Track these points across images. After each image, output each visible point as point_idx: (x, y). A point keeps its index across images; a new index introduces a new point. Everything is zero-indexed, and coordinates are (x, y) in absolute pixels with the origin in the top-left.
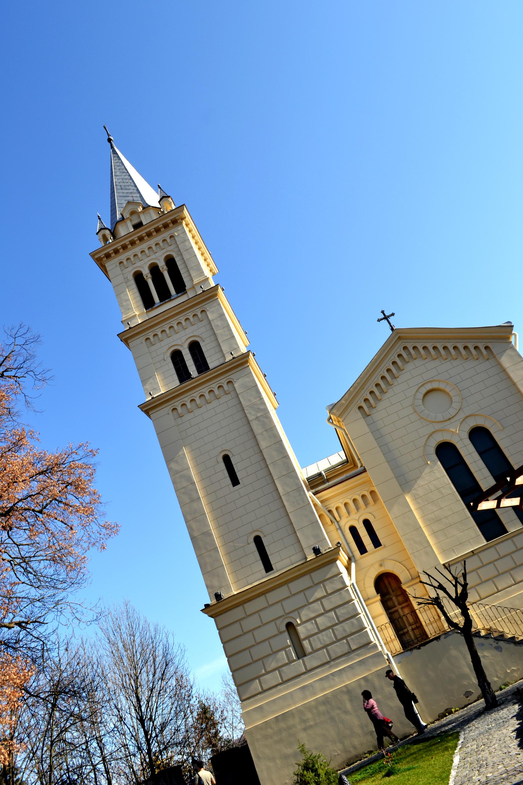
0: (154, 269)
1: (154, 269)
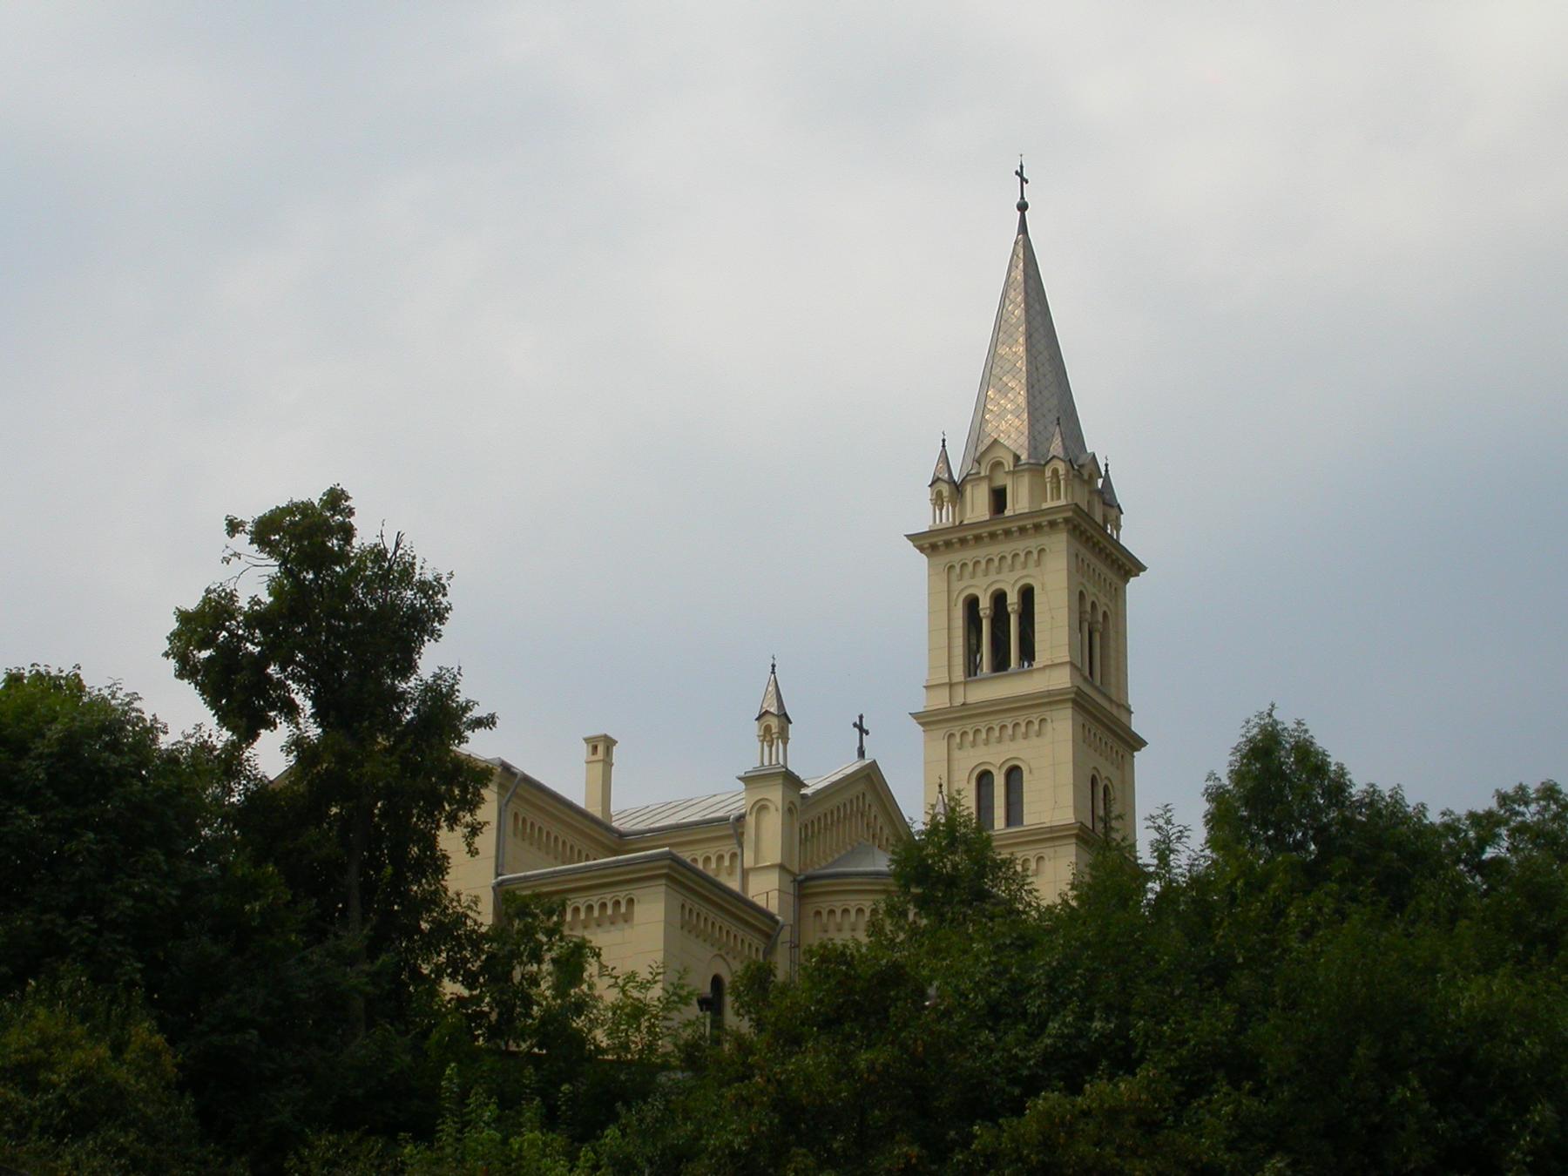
0: (999, 598)
1: (999, 598)
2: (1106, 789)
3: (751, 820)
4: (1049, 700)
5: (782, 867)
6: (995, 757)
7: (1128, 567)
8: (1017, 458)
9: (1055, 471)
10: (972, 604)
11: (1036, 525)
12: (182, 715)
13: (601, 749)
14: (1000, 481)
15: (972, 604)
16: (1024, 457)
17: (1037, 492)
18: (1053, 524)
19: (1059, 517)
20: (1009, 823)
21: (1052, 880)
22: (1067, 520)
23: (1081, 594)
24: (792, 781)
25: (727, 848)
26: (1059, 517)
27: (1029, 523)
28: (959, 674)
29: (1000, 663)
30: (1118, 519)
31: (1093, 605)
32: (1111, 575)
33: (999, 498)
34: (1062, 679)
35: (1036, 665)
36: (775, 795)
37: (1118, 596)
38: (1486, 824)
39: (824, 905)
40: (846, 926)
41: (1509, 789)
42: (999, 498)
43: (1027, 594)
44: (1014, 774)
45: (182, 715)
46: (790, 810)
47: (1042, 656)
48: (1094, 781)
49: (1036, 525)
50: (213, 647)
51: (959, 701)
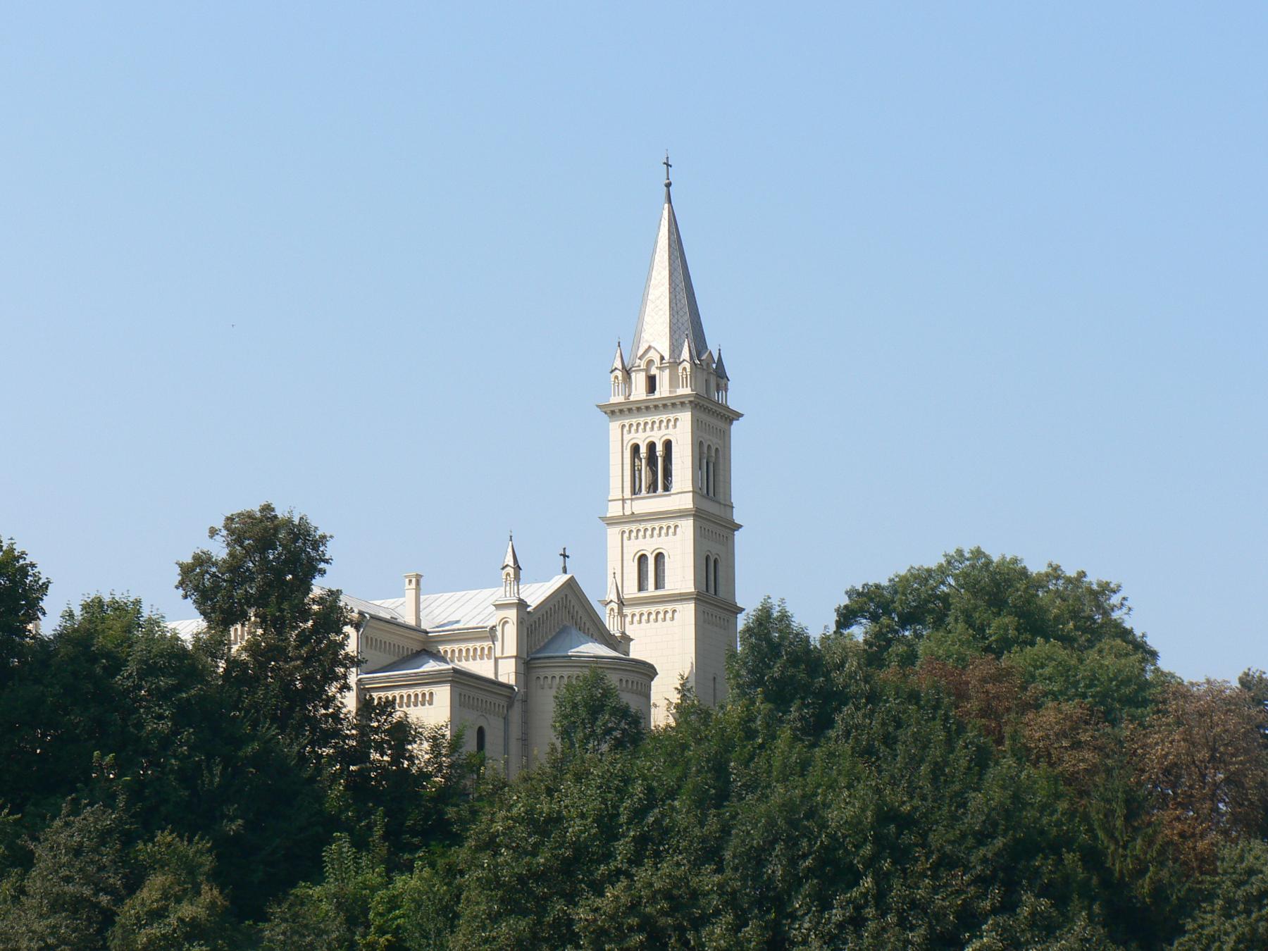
0: (652, 446)
1: (652, 446)
2: (716, 561)
3: (499, 629)
4: (681, 514)
5: (516, 657)
6: (649, 546)
7: (731, 416)
8: (662, 358)
9: (684, 369)
10: (636, 449)
11: (673, 404)
12: (187, 625)
13: (414, 580)
14: (654, 371)
15: (636, 449)
16: (667, 357)
17: (673, 383)
18: (682, 403)
19: (686, 400)
20: (657, 588)
21: (667, 647)
22: (691, 402)
23: (701, 443)
24: (522, 605)
25: (486, 644)
26: (686, 400)
27: (669, 403)
28: (628, 494)
29: (653, 487)
30: (726, 385)
31: (709, 446)
32: (721, 424)
33: (651, 383)
34: (687, 502)
35: (673, 491)
36: (512, 614)
37: (725, 436)
38: (942, 570)
39: (542, 673)
40: (555, 686)
41: (952, 552)
42: (651, 383)
43: (668, 445)
44: (659, 557)
45: (187, 625)
46: (520, 622)
47: (676, 487)
48: (707, 558)
49: (673, 404)
50: (199, 580)
51: (628, 512)
